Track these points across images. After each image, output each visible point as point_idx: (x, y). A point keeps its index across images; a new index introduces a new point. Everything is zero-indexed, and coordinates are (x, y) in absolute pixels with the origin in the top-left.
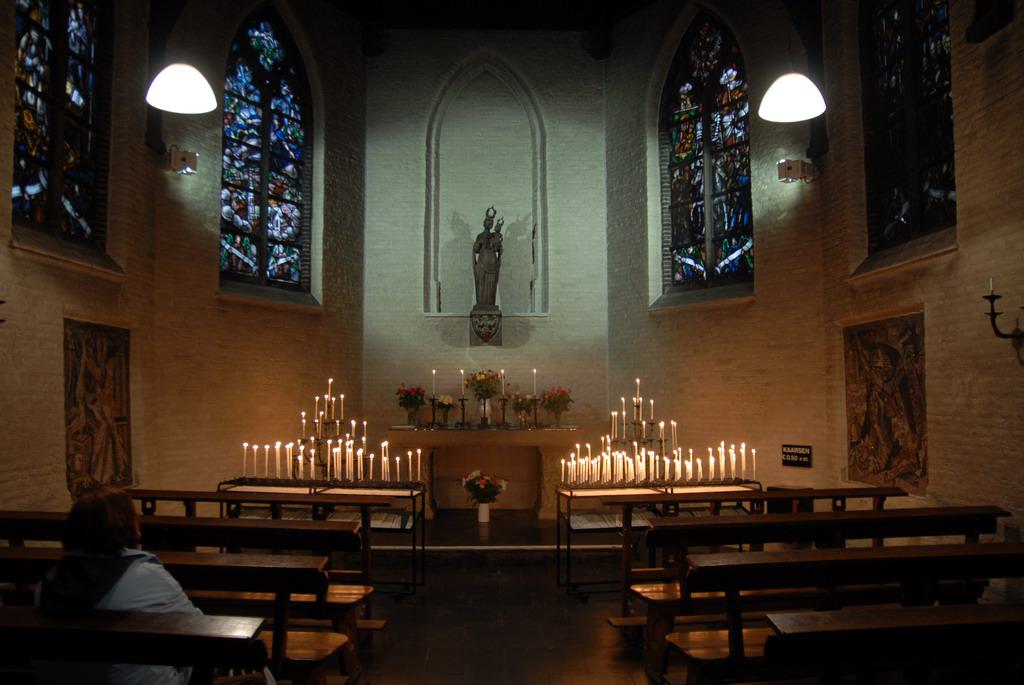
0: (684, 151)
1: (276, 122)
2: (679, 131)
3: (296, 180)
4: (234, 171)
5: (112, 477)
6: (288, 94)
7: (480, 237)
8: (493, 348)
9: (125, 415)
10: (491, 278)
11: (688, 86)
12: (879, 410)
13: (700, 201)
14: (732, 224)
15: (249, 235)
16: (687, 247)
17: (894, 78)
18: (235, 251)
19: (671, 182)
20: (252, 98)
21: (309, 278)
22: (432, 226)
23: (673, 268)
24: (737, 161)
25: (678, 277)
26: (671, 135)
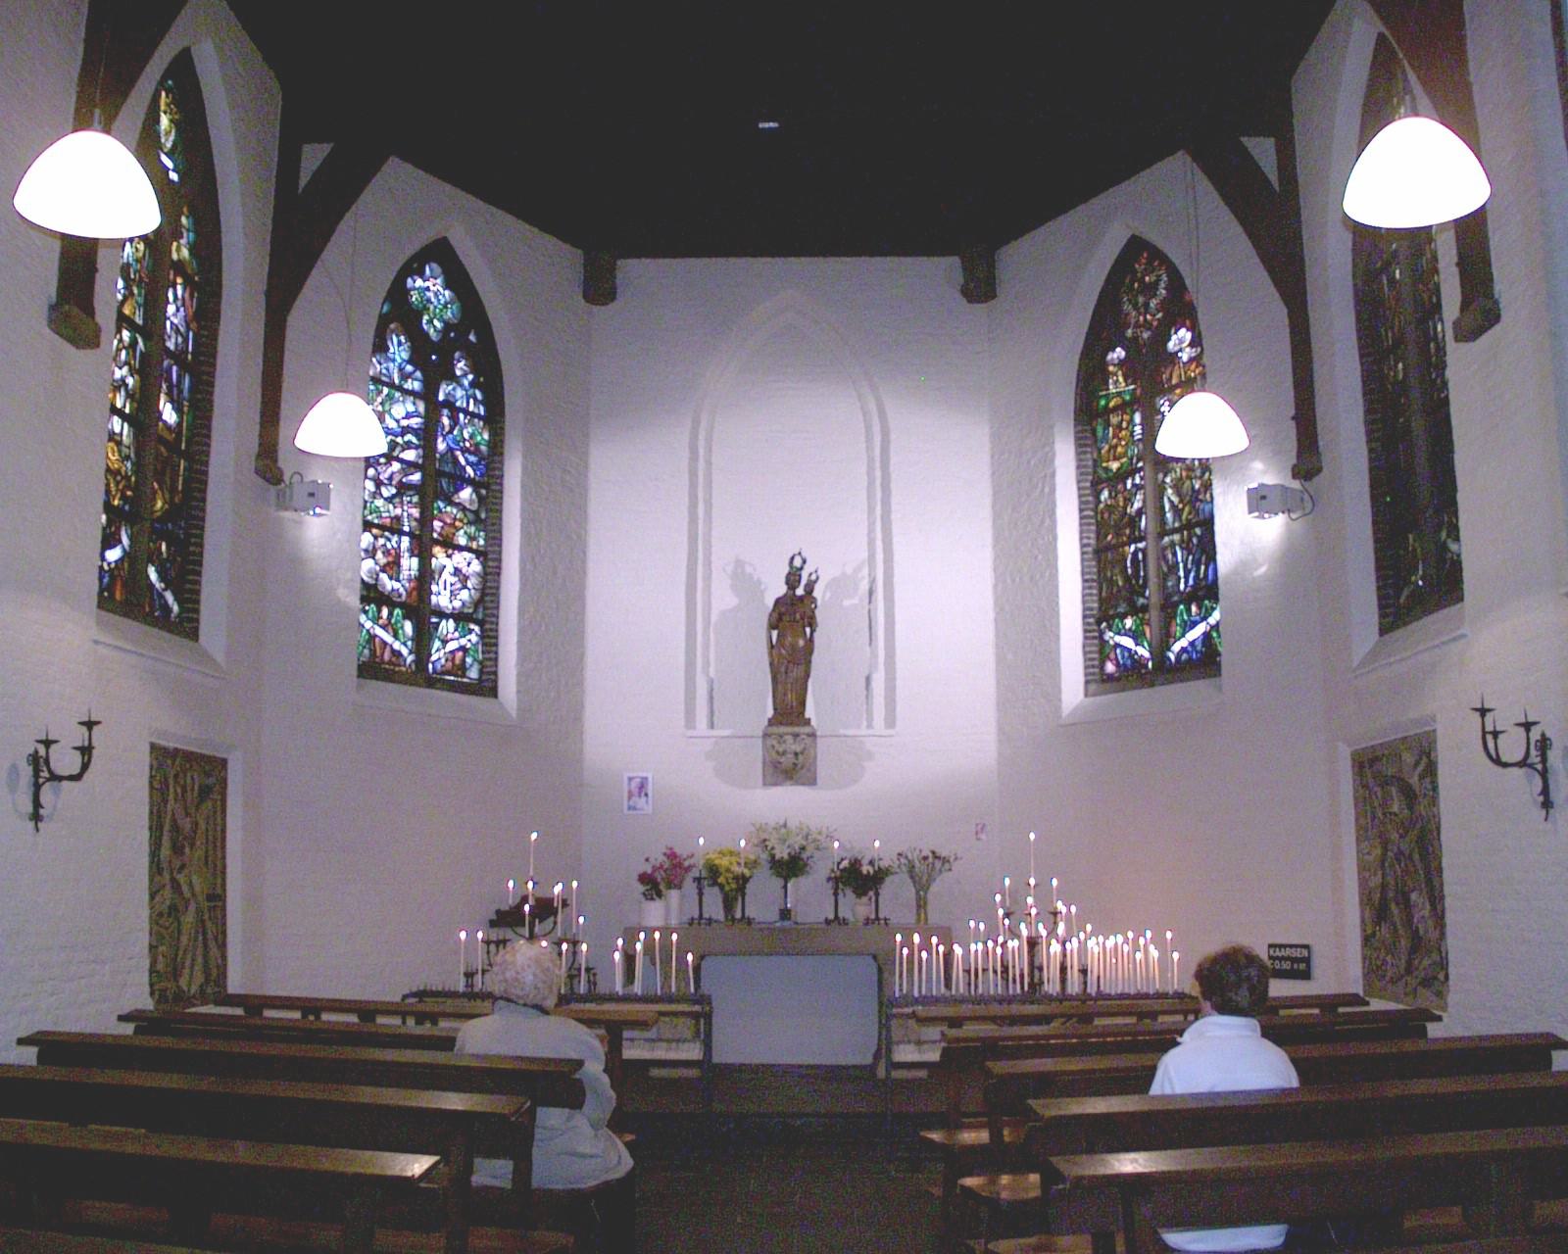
0: (1116, 459)
1: (446, 421)
2: (1108, 424)
3: (476, 513)
4: (379, 502)
5: (201, 986)
6: (465, 375)
7: (778, 601)
8: (801, 788)
9: (219, 891)
10: (797, 672)
11: (1119, 353)
12: (1396, 879)
13: (1140, 541)
14: (1191, 582)
15: (402, 605)
16: (1123, 617)
17: (1400, 365)
18: (379, 632)
19: (1095, 510)
20: (409, 385)
21: (495, 673)
22: (700, 584)
23: (1101, 652)
24: (1196, 477)
25: (1110, 667)
26: (1094, 432)
